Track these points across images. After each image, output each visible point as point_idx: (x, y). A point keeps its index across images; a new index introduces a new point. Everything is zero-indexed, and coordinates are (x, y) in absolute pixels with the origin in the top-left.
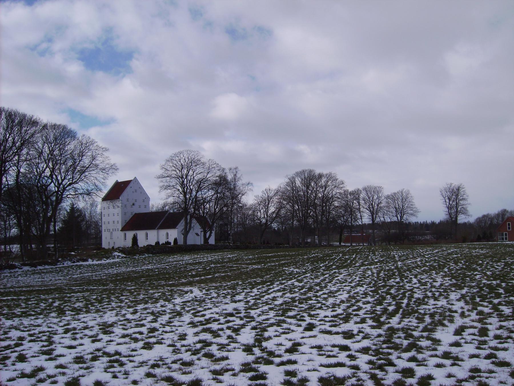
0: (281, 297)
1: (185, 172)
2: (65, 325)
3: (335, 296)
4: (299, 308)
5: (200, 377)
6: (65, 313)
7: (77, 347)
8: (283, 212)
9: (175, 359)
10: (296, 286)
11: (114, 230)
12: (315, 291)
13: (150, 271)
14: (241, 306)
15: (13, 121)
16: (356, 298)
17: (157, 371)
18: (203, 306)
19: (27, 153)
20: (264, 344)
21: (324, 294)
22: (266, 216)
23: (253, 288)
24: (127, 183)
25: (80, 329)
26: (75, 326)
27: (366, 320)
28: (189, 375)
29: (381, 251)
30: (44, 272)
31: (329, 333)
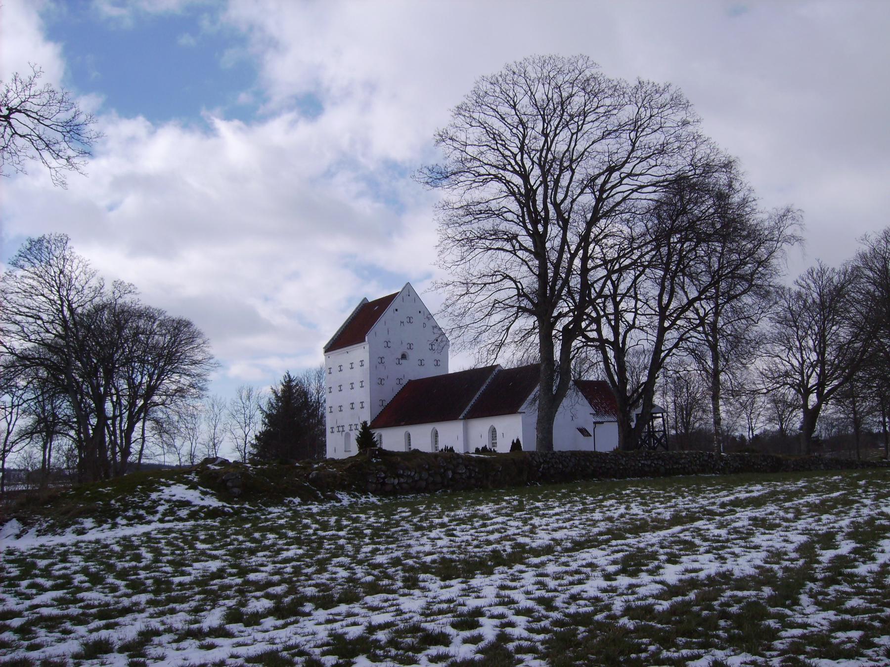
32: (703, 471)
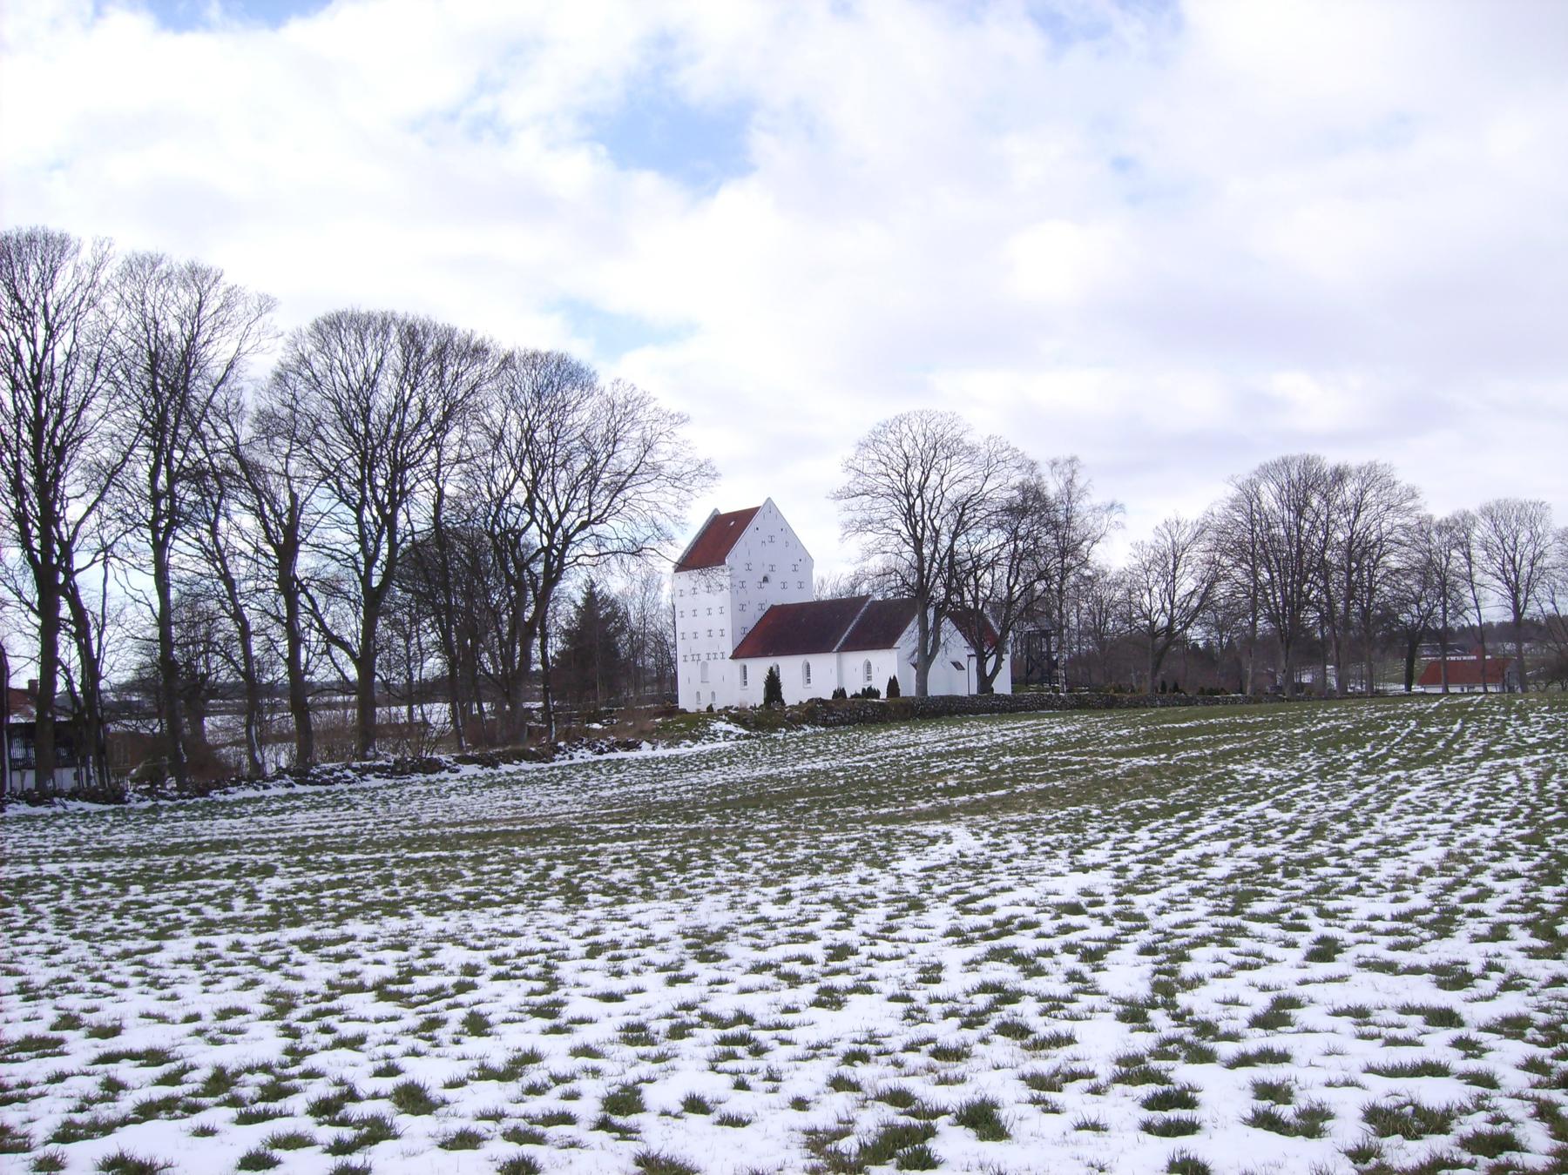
0: (1227, 855)
1: (917, 479)
2: (588, 934)
3: (1399, 854)
4: (1287, 889)
5: (991, 1094)
6: (586, 900)
7: (627, 997)
8: (1222, 589)
9: (915, 1038)
10: (1272, 821)
11: (712, 657)
12: (1336, 836)
13: (821, 777)
14: (1102, 881)
15: (420, 351)
16: (1472, 862)
17: (860, 1072)
18: (985, 880)
19: (461, 439)
20: (1183, 999)
21: (1366, 846)
22: (1168, 606)
23: (1138, 827)
24: (743, 519)
25: (631, 947)
26: (617, 936)
27: (1507, 930)
28: (958, 1087)
29: (1546, 711)
30: (518, 782)
31: (1389, 968)
32: (1043, 709)
